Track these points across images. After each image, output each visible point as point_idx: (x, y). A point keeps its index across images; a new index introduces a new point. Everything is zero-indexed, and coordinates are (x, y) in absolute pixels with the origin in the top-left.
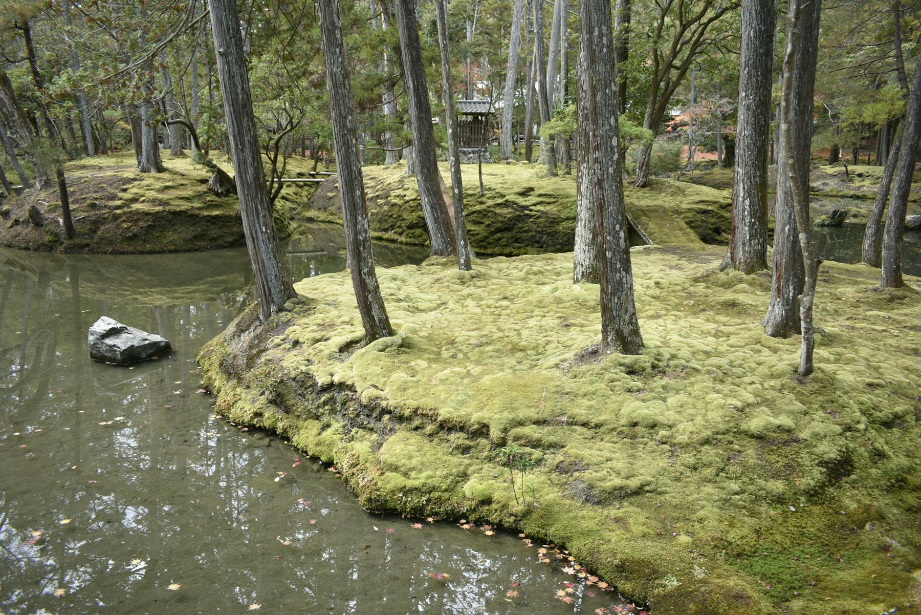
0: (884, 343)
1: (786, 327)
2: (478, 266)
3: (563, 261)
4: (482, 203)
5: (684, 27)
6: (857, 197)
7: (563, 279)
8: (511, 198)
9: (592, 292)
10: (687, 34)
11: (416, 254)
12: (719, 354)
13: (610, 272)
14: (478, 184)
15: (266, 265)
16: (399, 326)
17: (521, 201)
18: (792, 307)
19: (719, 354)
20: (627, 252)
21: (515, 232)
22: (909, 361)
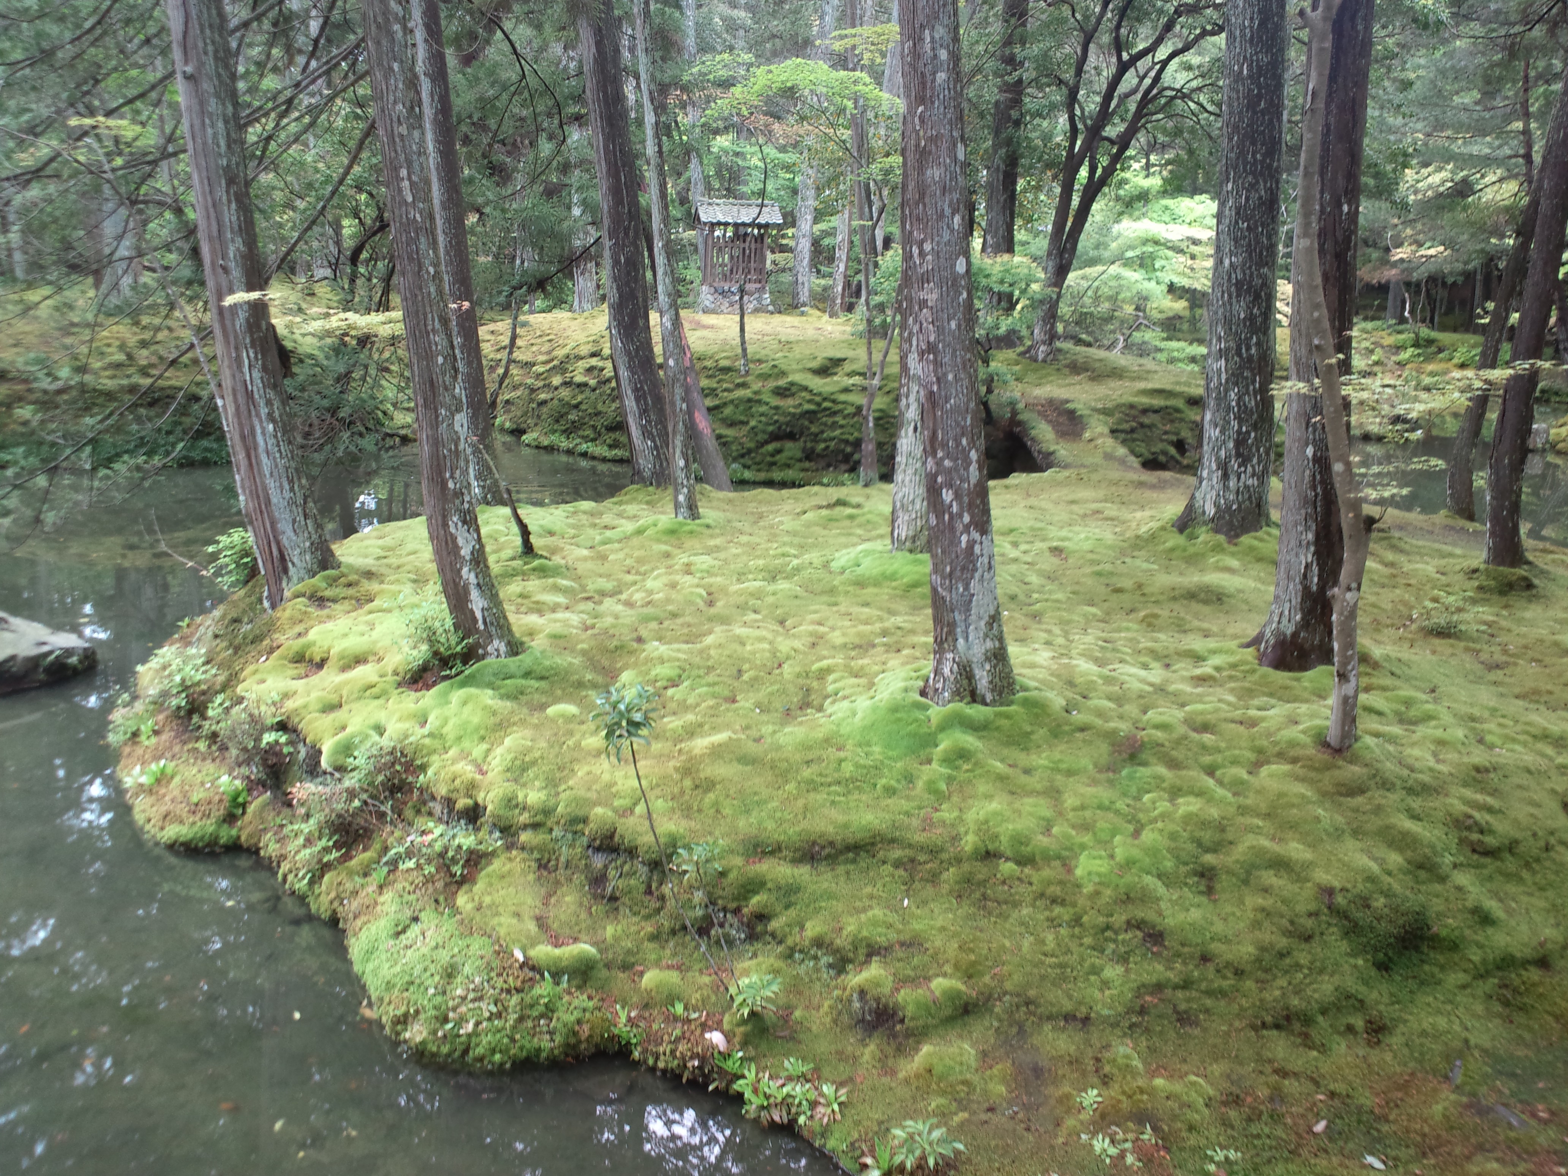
0: (1546, 699)
1: (1306, 643)
2: (716, 505)
3: (878, 501)
4: (744, 385)
5: (1123, 68)
6: (893, 521)
7: (855, 538)
8: (797, 378)
9: (919, 567)
10: (1130, 80)
11: (601, 479)
12: (1219, 751)
13: (953, 541)
14: (739, 351)
15: (274, 500)
16: (531, 634)
17: (817, 384)
18: (1317, 606)
19: (1219, 751)
20: (982, 493)
21: (800, 441)
22: (1542, 719)
